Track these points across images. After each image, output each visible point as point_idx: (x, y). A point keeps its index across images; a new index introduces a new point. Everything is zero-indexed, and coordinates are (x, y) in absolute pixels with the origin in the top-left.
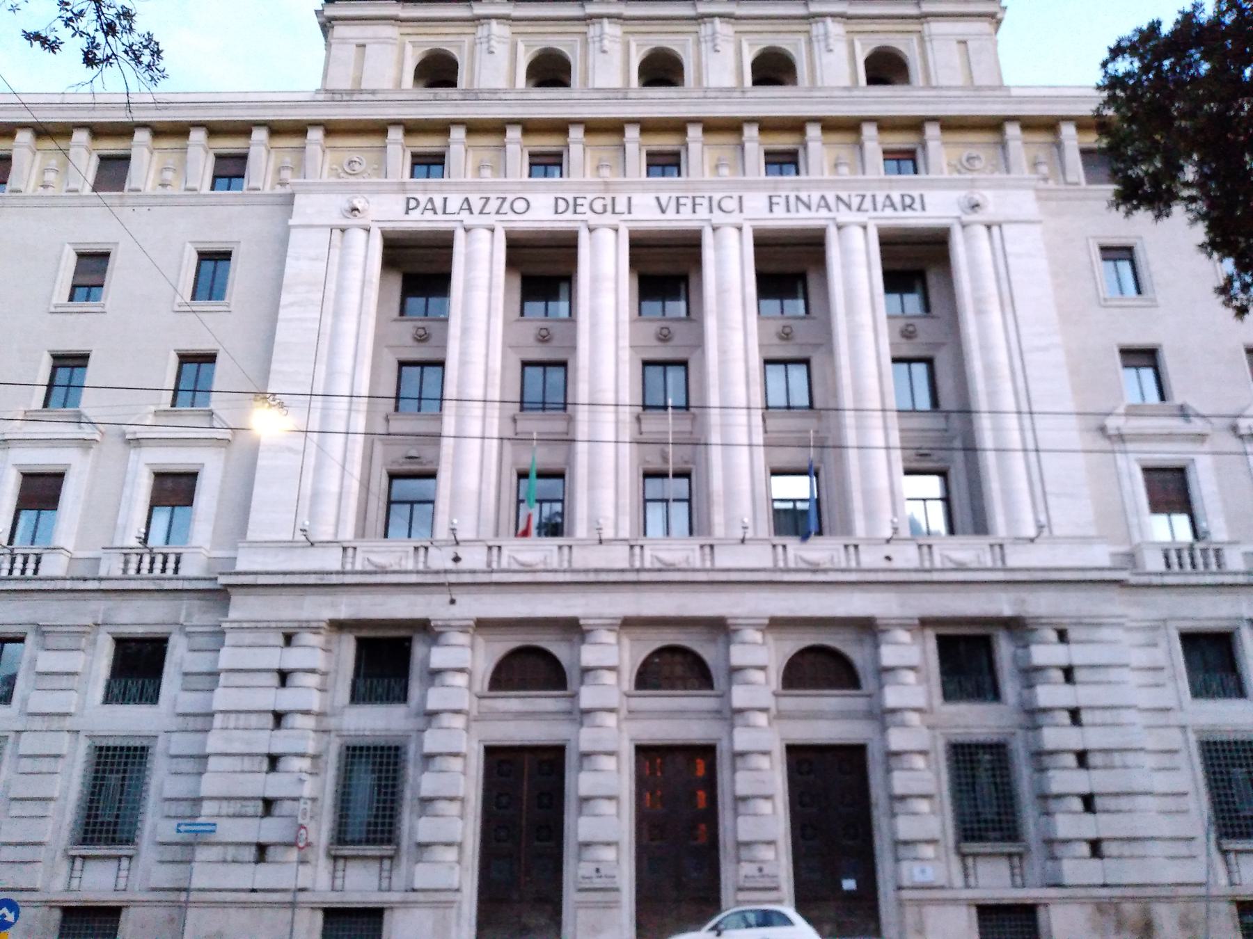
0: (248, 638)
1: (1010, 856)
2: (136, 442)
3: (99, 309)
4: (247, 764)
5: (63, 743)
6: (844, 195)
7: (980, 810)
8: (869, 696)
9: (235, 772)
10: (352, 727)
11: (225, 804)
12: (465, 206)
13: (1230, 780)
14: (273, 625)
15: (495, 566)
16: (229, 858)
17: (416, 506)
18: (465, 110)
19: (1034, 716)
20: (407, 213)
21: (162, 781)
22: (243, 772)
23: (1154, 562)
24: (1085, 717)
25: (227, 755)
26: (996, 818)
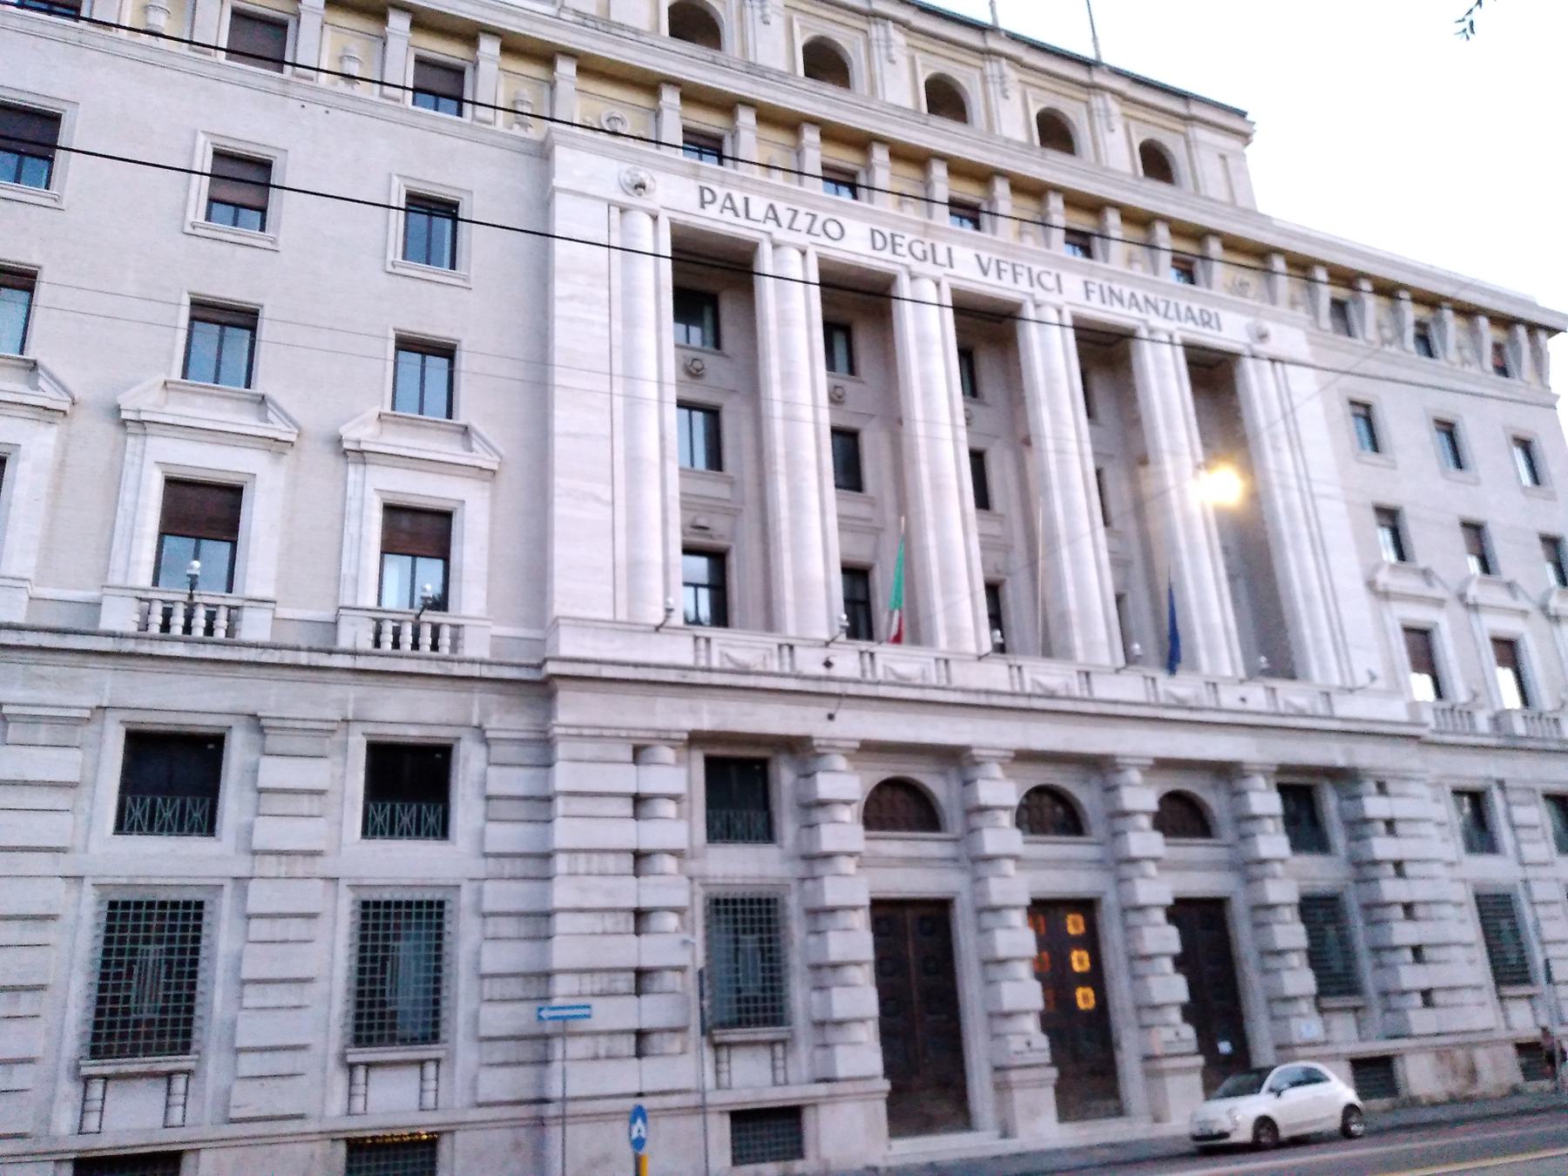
0: (589, 749)
1: (1356, 1009)
2: (361, 456)
4: (609, 922)
6: (1151, 297)
7: (741, 985)
8: (1229, 846)
9: (594, 934)
10: (720, 874)
11: (587, 978)
12: (771, 215)
13: (385, 959)
14: (623, 733)
15: (869, 676)
16: (602, 1052)
18: (763, 90)
19: (1364, 868)
20: (702, 206)
21: (469, 946)
22: (604, 933)
23: (356, 634)
24: (1409, 869)
25: (581, 910)
26: (760, 994)
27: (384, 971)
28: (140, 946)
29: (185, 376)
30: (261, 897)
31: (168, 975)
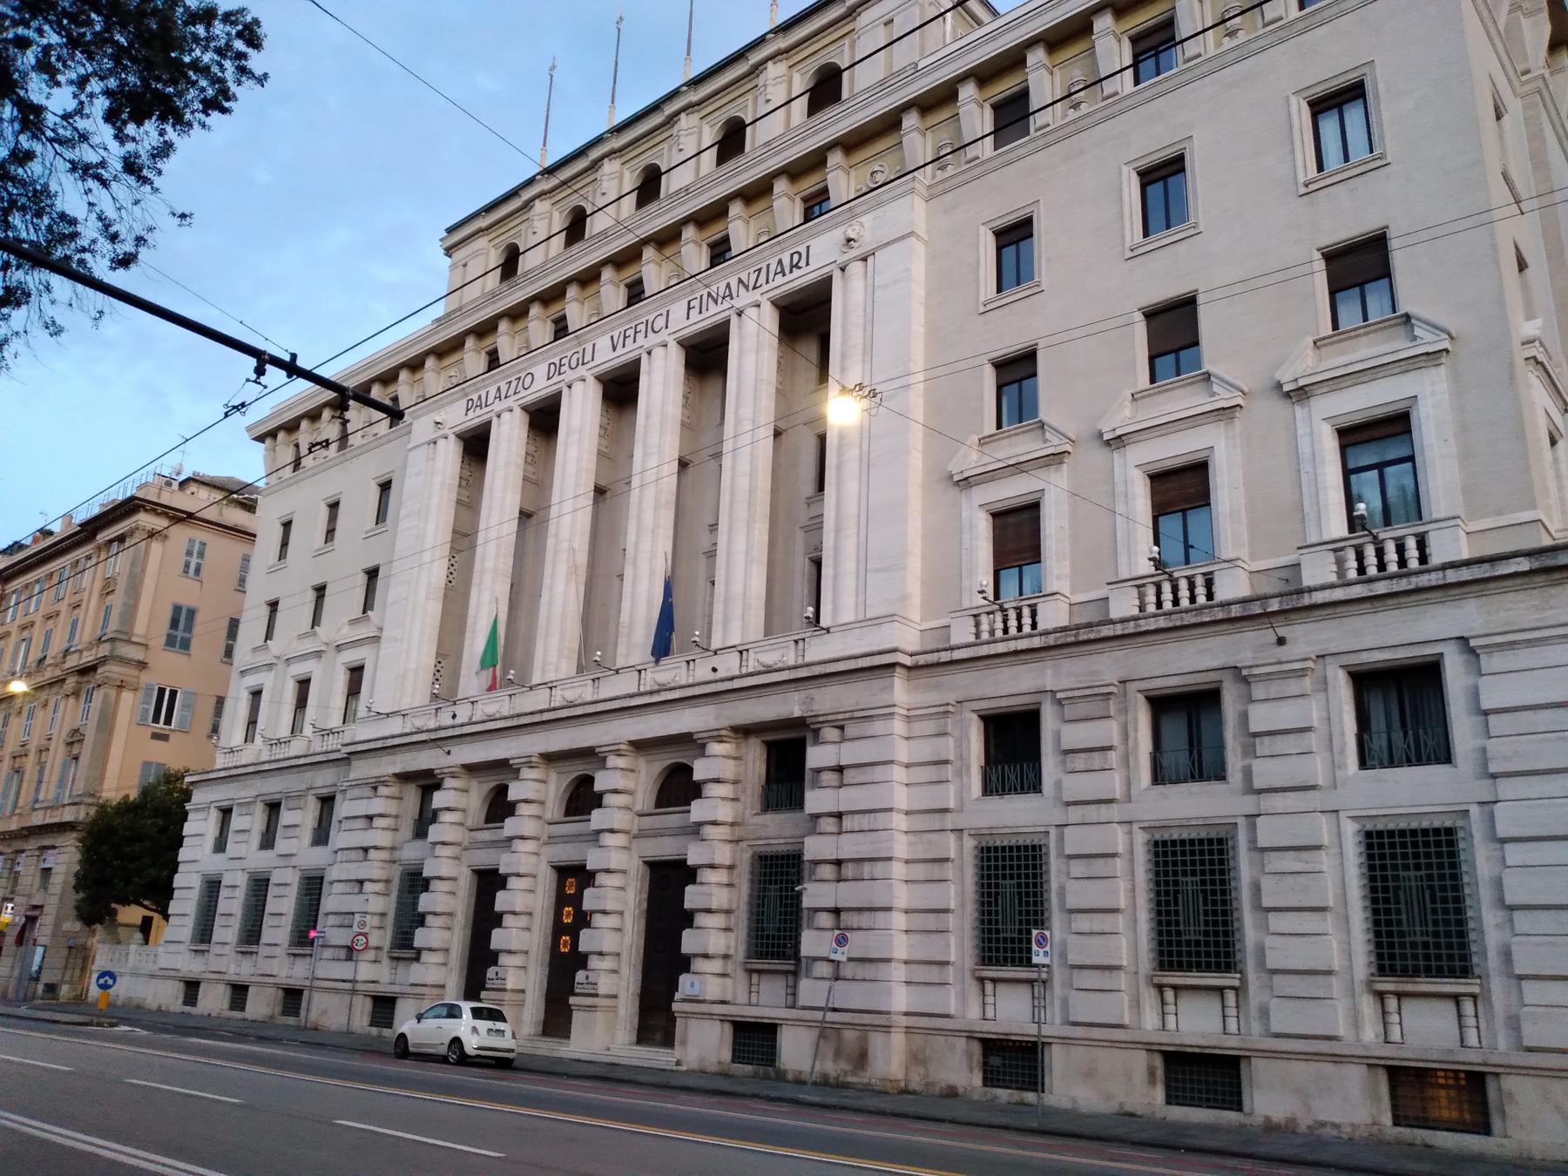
1: (1456, 998)
3: (1192, 232)
5: (1118, 839)
13: (997, 894)
17: (1389, 470)
23: (962, 633)
27: (1176, 904)
28: (1180, 878)
29: (1153, 381)
30: (1075, 840)
31: (1433, 901)
